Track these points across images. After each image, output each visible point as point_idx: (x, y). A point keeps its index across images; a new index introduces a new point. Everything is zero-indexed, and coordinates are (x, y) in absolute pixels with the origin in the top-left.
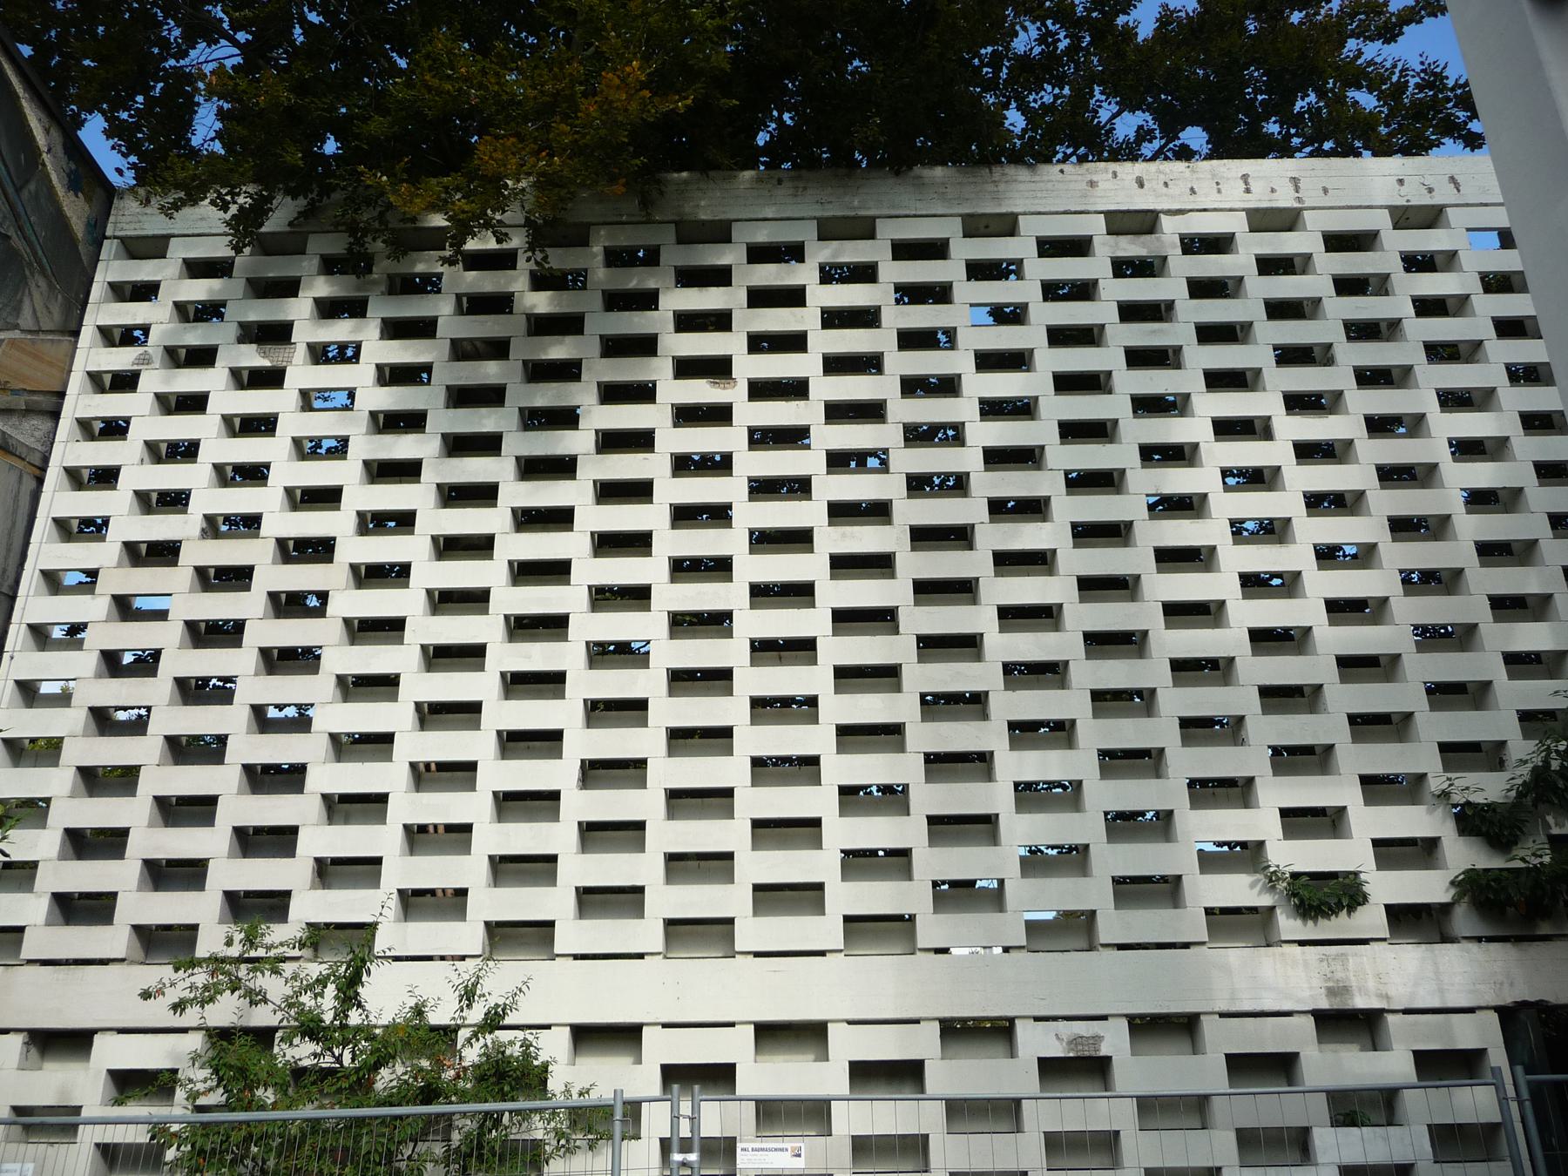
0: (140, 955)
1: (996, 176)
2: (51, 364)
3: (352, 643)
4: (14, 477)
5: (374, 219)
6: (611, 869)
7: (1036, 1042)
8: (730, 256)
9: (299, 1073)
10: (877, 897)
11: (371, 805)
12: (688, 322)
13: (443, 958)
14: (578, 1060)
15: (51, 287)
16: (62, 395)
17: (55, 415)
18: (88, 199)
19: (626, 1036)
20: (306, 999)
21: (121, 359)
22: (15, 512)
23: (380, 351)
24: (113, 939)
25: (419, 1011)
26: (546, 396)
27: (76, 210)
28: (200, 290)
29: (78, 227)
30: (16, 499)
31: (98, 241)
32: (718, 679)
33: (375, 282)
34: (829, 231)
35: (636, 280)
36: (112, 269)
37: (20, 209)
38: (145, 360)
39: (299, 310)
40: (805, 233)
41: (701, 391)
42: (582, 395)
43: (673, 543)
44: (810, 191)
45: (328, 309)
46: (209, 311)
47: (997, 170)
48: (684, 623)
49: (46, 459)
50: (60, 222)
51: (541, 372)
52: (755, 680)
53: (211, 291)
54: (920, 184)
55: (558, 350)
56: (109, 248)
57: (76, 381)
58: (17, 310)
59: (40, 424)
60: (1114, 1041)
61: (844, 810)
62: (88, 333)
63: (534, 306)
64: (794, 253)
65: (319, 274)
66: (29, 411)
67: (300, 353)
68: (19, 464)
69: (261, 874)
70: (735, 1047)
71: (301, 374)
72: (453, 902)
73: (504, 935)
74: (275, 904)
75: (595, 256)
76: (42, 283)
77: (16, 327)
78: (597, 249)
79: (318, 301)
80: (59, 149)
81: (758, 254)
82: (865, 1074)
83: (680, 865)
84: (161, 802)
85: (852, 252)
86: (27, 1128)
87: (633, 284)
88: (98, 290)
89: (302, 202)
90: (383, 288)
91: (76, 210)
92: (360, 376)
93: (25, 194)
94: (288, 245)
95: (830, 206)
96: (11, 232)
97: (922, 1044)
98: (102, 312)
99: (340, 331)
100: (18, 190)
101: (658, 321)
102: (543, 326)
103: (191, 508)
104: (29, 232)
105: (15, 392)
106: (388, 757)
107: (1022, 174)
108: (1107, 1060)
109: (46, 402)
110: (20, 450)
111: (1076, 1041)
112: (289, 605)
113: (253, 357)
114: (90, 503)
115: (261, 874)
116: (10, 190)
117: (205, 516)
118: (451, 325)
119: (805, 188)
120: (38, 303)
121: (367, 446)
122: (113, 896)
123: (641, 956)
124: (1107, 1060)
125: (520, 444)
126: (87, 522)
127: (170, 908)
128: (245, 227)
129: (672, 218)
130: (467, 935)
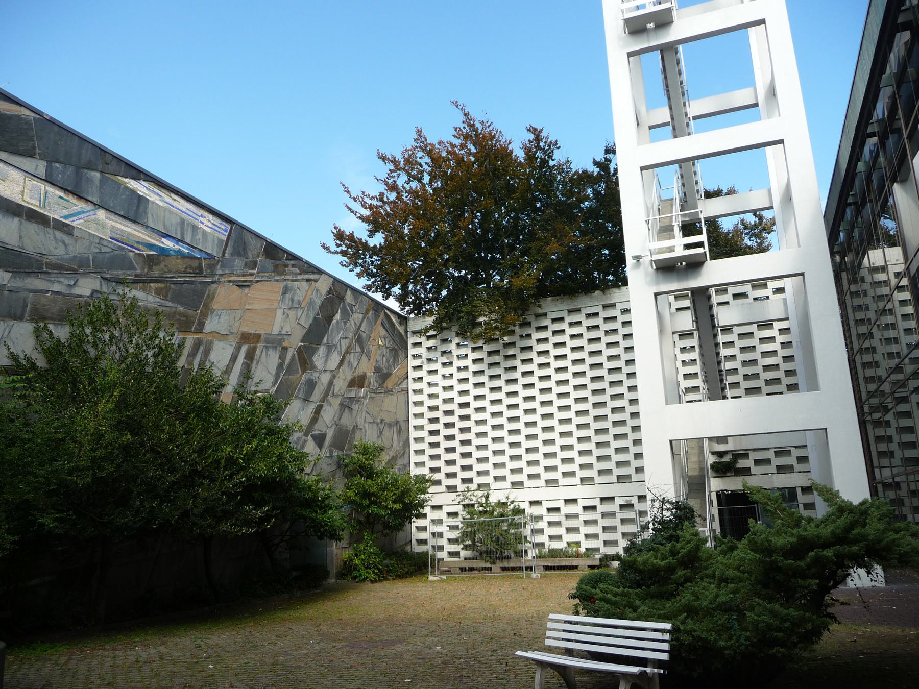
1: (610, 292)
7: (619, 501)
8: (546, 322)
9: (481, 512)
10: (586, 473)
17: (408, 377)
19: (538, 503)
20: (480, 500)
21: (417, 362)
25: (499, 501)
27: (401, 329)
29: (402, 332)
31: (406, 332)
34: (570, 312)
39: (453, 346)
40: (564, 314)
42: (517, 363)
47: (610, 290)
51: (507, 357)
56: (409, 334)
57: (410, 369)
60: (634, 501)
61: (745, 380)
62: (410, 357)
66: (404, 380)
67: (455, 358)
68: (404, 392)
70: (560, 504)
72: (503, 478)
73: (514, 484)
74: (470, 480)
76: (400, 351)
82: (586, 508)
83: (562, 434)
85: (575, 318)
97: (596, 502)
98: (412, 351)
101: (532, 342)
107: (616, 290)
108: (633, 504)
111: (627, 501)
113: (445, 360)
114: (418, 374)
115: (467, 475)
121: (473, 380)
124: (633, 504)
125: (505, 377)
127: (451, 482)
130: (507, 484)
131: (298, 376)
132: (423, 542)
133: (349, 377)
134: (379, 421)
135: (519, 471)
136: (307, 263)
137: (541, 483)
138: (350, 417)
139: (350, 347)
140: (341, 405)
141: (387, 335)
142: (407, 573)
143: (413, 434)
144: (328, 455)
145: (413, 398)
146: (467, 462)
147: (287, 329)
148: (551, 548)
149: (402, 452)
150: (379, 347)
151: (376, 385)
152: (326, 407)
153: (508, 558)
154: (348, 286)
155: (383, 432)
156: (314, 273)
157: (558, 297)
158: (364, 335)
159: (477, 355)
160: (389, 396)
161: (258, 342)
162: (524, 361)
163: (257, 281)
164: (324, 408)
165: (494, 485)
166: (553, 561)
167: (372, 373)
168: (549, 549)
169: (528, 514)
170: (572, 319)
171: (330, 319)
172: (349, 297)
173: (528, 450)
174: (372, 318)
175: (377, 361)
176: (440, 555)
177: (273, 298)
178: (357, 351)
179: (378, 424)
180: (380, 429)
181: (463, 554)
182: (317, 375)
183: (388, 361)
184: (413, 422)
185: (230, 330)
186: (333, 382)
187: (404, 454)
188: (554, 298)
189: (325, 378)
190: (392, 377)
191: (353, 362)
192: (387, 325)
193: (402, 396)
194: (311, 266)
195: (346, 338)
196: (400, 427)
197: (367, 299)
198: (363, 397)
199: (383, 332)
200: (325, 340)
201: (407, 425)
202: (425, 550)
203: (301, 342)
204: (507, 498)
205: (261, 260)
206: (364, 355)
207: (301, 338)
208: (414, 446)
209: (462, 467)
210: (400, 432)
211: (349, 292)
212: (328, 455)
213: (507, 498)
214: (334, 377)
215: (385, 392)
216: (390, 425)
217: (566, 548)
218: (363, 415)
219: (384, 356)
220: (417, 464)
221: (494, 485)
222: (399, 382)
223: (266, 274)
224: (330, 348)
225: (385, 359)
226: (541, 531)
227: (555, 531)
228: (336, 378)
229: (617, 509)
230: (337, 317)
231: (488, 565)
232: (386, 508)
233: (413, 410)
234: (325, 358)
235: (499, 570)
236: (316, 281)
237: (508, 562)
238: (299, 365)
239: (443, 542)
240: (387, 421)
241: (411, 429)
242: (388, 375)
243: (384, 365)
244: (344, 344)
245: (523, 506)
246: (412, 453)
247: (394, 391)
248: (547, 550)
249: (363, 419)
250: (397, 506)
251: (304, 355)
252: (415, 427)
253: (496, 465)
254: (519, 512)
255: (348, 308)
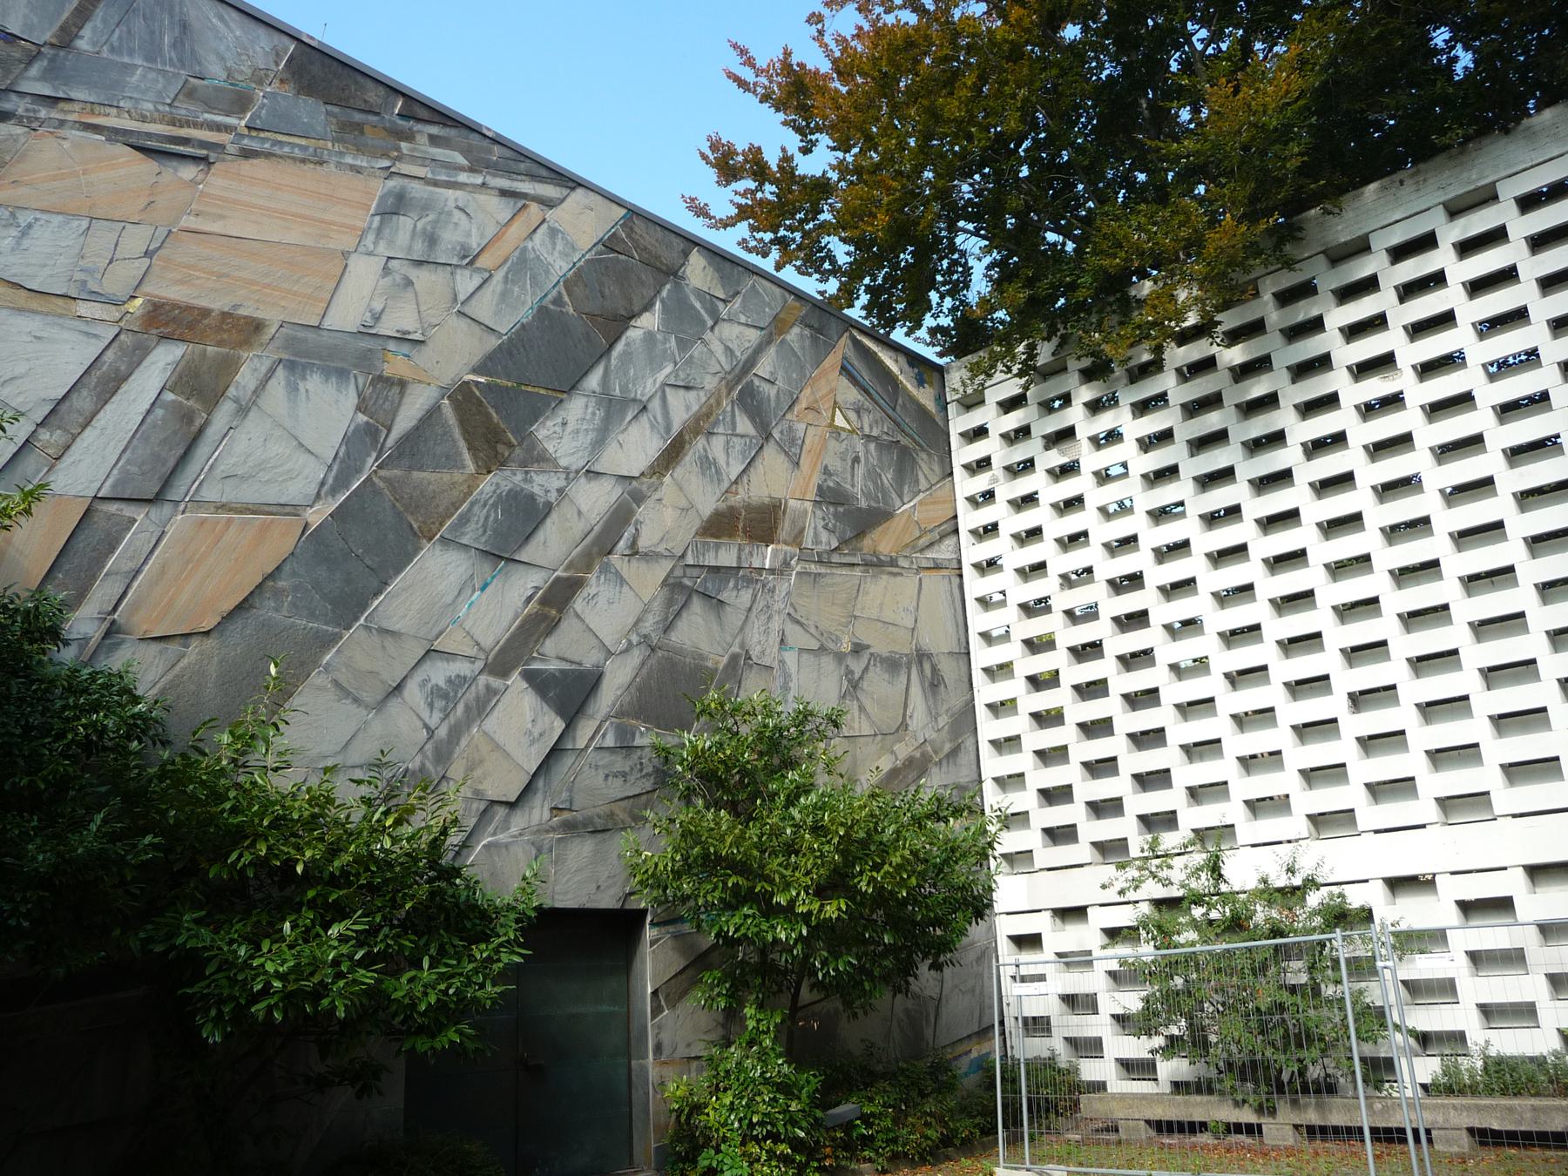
0: (1100, 859)
2: (944, 502)
3: (1157, 525)
4: (947, 580)
5: (1196, 873)
6: (1387, 767)
11: (1211, 746)
12: (1354, 332)
13: (1289, 842)
14: (1398, 900)
15: (929, 454)
16: (956, 517)
17: (956, 531)
18: (931, 384)
21: (981, 483)
22: (953, 601)
23: (1135, 428)
24: (1080, 851)
26: (1260, 426)
27: (925, 397)
28: (1014, 420)
29: (931, 406)
30: (952, 594)
31: (943, 405)
32: (1458, 704)
33: (1117, 379)
34: (1455, 211)
35: (1304, 311)
36: (959, 423)
37: (899, 419)
38: (995, 480)
39: (1075, 415)
41: (1376, 387)
42: (1284, 418)
43: (1389, 557)
44: (1431, 181)
45: (1095, 407)
46: (1023, 432)
48: (1405, 575)
49: (960, 562)
50: (922, 410)
51: (1253, 408)
52: (1480, 654)
53: (1019, 420)
54: (1532, 135)
55: (1258, 388)
56: (952, 409)
57: (962, 507)
58: (917, 481)
59: (950, 542)
62: (958, 472)
63: (1231, 360)
64: (1428, 242)
65: (1082, 384)
66: (943, 537)
68: (945, 572)
69: (1156, 802)
70: (1512, 884)
71: (1092, 460)
73: (1319, 821)
74: (1168, 820)
75: (1266, 303)
76: (924, 456)
77: (920, 491)
78: (1267, 297)
79: (1086, 405)
80: (906, 367)
81: (1399, 253)
84: (1077, 688)
86: (1067, 964)
87: (1301, 317)
88: (955, 440)
89: (1055, 341)
90: (1125, 381)
91: (925, 397)
92: (1126, 450)
93: (898, 408)
94: (1056, 369)
95: (1452, 188)
96: (900, 438)
98: (963, 454)
99: (1105, 421)
100: (894, 410)
101: (1329, 341)
102: (1245, 371)
103: (1058, 646)
104: (907, 430)
105: (930, 531)
106: (1195, 592)
109: (948, 527)
110: (945, 564)
112: (1131, 661)
113: (1056, 458)
114: (985, 516)
115: (1156, 802)
116: (890, 412)
117: (1060, 576)
118: (1180, 393)
119: (1425, 180)
120: (926, 468)
122: (1070, 786)
123: (1423, 826)
126: (1001, 667)
127: (1108, 829)
128: (1028, 369)
129: (1319, 249)
131: (458, 476)
132: (1037, 1026)
133: (708, 502)
134: (846, 647)
135: (1334, 773)
136: (497, 141)
137: (1423, 808)
138: (715, 627)
139: (708, 415)
140: (673, 586)
141: (868, 404)
142: (946, 1141)
143: (986, 692)
144: (610, 741)
145: (975, 586)
146: (1151, 760)
147: (401, 319)
148: (1493, 1052)
149: (947, 747)
150: (836, 431)
151: (828, 541)
152: (596, 585)
153: (1328, 1087)
154: (692, 242)
155: (865, 684)
156: (534, 177)
157: (1400, 175)
158: (770, 391)
159: (1152, 423)
160: (885, 577)
161: (246, 343)
162: (1310, 408)
163: (247, 154)
164: (590, 589)
165: (1249, 829)
166: (1510, 1109)
167: (809, 506)
168: (1486, 1058)
169: (1383, 924)
170: (1465, 229)
171: (618, 323)
172: (697, 271)
173: (1359, 700)
174: (803, 348)
175: (826, 471)
176: (1090, 1070)
177: (329, 217)
178: (740, 430)
179: (840, 657)
180: (849, 672)
181: (1170, 1069)
182: (556, 482)
183: (872, 475)
184: (982, 656)
185: (84, 283)
186: (631, 513)
187: (955, 752)
188: (1386, 181)
189: (595, 500)
190: (895, 525)
191: (722, 461)
192: (865, 375)
193: (936, 584)
194: (521, 154)
195: (687, 388)
196: (934, 670)
197: (777, 290)
198: (772, 571)
199: (851, 394)
200: (593, 381)
201: (964, 669)
202: (1046, 1054)
203: (475, 371)
204: (1291, 870)
205: (272, 96)
206: (770, 451)
207: (476, 359)
208: (989, 728)
209: (1138, 778)
210: (934, 684)
211: (696, 260)
212: (610, 741)
213: (1291, 870)
214: (638, 498)
215: (867, 564)
216: (892, 664)
217: (1556, 1054)
218: (776, 624)
219: (856, 460)
220: (1002, 782)
221: (1249, 829)
222: (923, 542)
223: (303, 142)
224: (615, 409)
225: (860, 471)
226: (1445, 989)
227: (1503, 988)
228: (650, 503)
229: (1447, 916)
230: (650, 321)
231: (1247, 1116)
232: (788, 911)
233: (978, 621)
234: (591, 436)
235: (1289, 1138)
236: (549, 204)
237: (1320, 1107)
238: (462, 445)
239: (1098, 1026)
240: (880, 647)
241: (978, 677)
242: (877, 517)
243: (858, 486)
244: (682, 408)
245: (1356, 898)
246: (985, 750)
247: (903, 563)
248: (1479, 1064)
249: (774, 639)
250: (832, 909)
251: (488, 415)
252: (987, 670)
253: (1249, 763)
254: (1341, 917)
255: (698, 305)
